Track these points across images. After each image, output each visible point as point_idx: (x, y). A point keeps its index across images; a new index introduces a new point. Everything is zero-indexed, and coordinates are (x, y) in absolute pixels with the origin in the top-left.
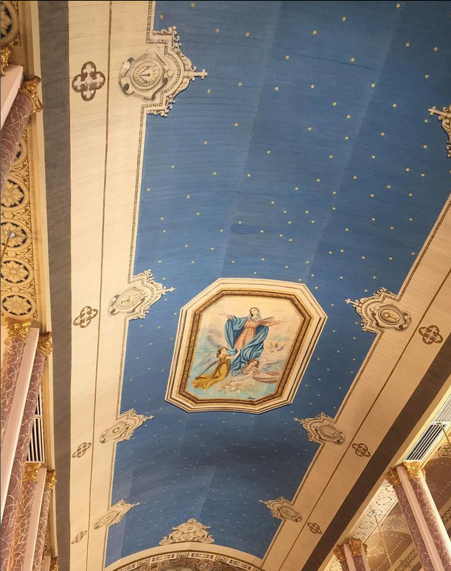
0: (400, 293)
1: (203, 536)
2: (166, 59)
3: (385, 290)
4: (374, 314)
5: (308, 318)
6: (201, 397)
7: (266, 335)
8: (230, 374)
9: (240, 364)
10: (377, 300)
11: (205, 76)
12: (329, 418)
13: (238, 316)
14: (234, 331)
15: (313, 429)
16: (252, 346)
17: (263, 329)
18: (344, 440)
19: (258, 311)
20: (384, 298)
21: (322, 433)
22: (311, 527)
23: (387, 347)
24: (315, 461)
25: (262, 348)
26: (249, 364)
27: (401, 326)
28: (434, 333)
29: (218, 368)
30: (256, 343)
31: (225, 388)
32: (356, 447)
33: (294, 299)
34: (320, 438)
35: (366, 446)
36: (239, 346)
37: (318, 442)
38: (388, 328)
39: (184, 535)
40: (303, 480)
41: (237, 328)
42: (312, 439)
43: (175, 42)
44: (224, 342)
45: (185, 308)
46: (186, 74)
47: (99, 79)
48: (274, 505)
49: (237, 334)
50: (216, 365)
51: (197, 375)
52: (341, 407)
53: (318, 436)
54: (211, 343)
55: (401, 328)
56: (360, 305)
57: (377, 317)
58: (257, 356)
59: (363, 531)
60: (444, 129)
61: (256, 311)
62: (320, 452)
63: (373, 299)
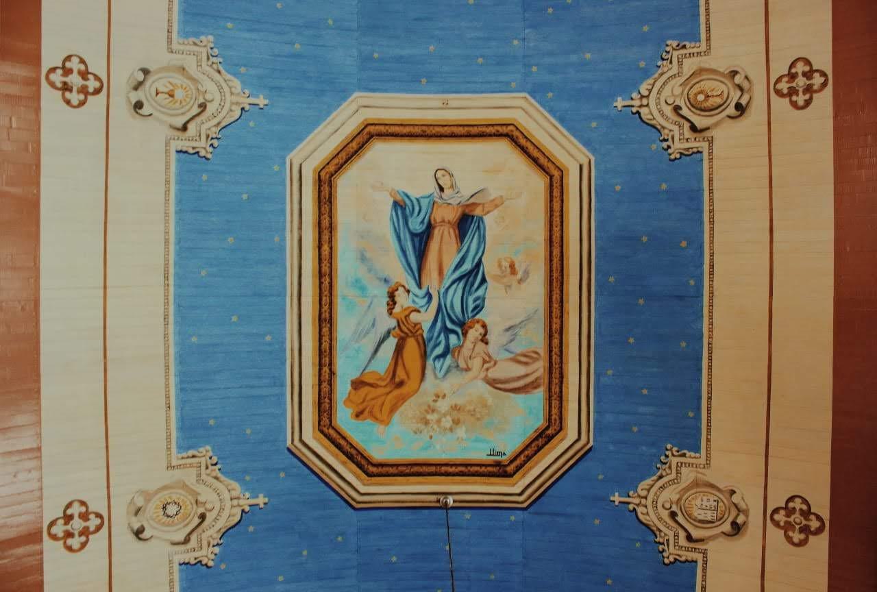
0: (703, 36)
2: (200, 488)
3: (675, 44)
4: (677, 109)
5: (556, 173)
6: (378, 452)
7: (482, 240)
8: (429, 372)
9: (447, 339)
10: (670, 73)
11: (265, 504)
13: (414, 194)
14: (413, 235)
16: (460, 279)
17: (473, 226)
19: (451, 175)
20: (680, 63)
21: (689, 516)
25: (484, 281)
26: (465, 334)
27: (739, 107)
28: (804, 74)
29: (399, 350)
30: (467, 266)
31: (427, 423)
32: (781, 517)
33: (516, 133)
36: (431, 280)
38: (717, 124)
41: (416, 225)
42: (671, 553)
43: (213, 56)
44: (399, 273)
45: (295, 156)
46: (235, 99)
47: (93, 522)
49: (422, 241)
50: (392, 342)
51: (355, 375)
53: (682, 534)
54: (370, 270)
55: (737, 529)
56: (645, 102)
57: (685, 111)
58: (478, 308)
61: (447, 177)
63: (662, 74)
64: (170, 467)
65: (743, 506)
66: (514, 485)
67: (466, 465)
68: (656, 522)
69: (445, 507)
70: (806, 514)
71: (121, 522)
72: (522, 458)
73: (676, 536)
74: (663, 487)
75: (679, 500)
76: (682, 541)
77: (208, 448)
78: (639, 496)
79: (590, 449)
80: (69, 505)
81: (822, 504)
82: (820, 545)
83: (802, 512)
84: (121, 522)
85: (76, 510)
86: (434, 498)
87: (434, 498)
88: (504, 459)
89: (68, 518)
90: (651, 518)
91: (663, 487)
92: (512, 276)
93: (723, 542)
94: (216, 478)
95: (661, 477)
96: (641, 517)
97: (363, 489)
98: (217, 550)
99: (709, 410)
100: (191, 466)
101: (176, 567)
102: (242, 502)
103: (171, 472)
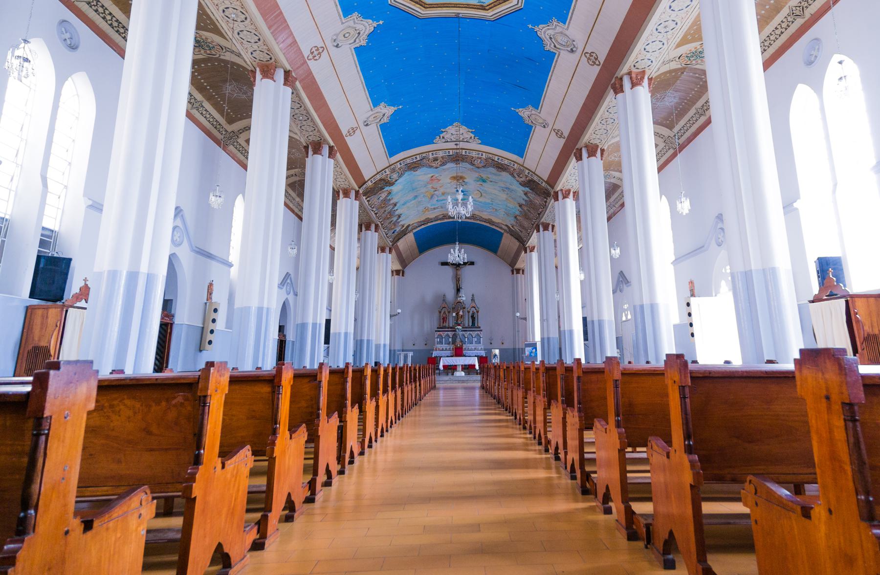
1: (471, 138)
12: (561, 24)
15: (548, 37)
18: (577, 48)
20: (556, 26)
21: (557, 41)
22: (557, 133)
23: (564, 64)
24: (553, 71)
32: (588, 55)
34: (555, 46)
35: (596, 55)
37: (554, 51)
39: (455, 136)
40: (545, 90)
42: (547, 48)
47: (321, 50)
48: (524, 113)
52: (571, 11)
53: (553, 45)
59: (648, 56)
60: (538, 36)
62: (557, 61)
64: (343, 23)
65: (576, 46)
66: (488, 13)
67: (468, 5)
68: (544, 38)
69: (458, 17)
70: (596, 59)
71: (329, 44)
72: (493, 5)
73: (550, 44)
74: (548, 29)
75: (554, 35)
76: (552, 46)
77: (356, 13)
78: (539, 28)
79: (522, 8)
80: (320, 57)
81: (602, 59)
82: (597, 69)
83: (595, 58)
84: (329, 44)
85: (314, 49)
86: (454, 14)
87: (454, 14)
88: (485, 5)
89: (312, 53)
90: (542, 36)
91: (548, 29)
92: (756, 547)
93: (567, 53)
94: (362, 21)
95: (549, 26)
96: (538, 34)
97: (423, 12)
98: (367, 41)
99: (572, 14)
100: (351, 20)
101: (353, 50)
102: (373, 25)
103: (343, 25)
